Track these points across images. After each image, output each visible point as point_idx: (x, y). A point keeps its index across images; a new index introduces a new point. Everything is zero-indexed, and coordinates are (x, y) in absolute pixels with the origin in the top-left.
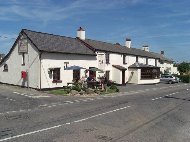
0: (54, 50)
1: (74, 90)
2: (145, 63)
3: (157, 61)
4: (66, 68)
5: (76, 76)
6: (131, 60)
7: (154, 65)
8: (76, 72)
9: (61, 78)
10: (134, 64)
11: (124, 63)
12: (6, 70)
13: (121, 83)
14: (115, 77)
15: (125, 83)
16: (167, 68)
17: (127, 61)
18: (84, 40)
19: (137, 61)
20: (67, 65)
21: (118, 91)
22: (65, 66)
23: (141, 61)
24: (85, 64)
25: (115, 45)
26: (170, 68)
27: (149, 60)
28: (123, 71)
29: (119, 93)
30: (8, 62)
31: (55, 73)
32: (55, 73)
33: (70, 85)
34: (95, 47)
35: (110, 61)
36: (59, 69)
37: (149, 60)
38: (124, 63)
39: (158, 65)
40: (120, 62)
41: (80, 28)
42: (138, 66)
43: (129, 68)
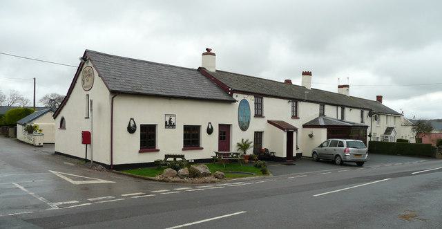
0: (144, 91)
1: (170, 169)
2: (340, 118)
3: (366, 113)
4: (170, 125)
5: (224, 138)
6: (309, 111)
7: (336, 118)
8: (192, 137)
9: (159, 145)
10: (316, 120)
11: (295, 116)
12: (62, 125)
13: (285, 155)
14: (276, 143)
15: (294, 155)
16: (388, 128)
17: (300, 114)
18: (213, 73)
19: (322, 114)
20: (171, 119)
21: (264, 172)
22: (166, 122)
23: (332, 113)
24: (206, 116)
25: (284, 85)
26: (393, 128)
27: (347, 110)
28: (290, 132)
29: (267, 177)
30: (63, 113)
31: (148, 137)
32: (148, 137)
33: (169, 159)
34: (232, 86)
35: (265, 114)
36: (197, 128)
37: (347, 110)
38: (295, 116)
39: (367, 122)
40: (286, 117)
41: (304, 74)
42: (322, 123)
43: (305, 126)
